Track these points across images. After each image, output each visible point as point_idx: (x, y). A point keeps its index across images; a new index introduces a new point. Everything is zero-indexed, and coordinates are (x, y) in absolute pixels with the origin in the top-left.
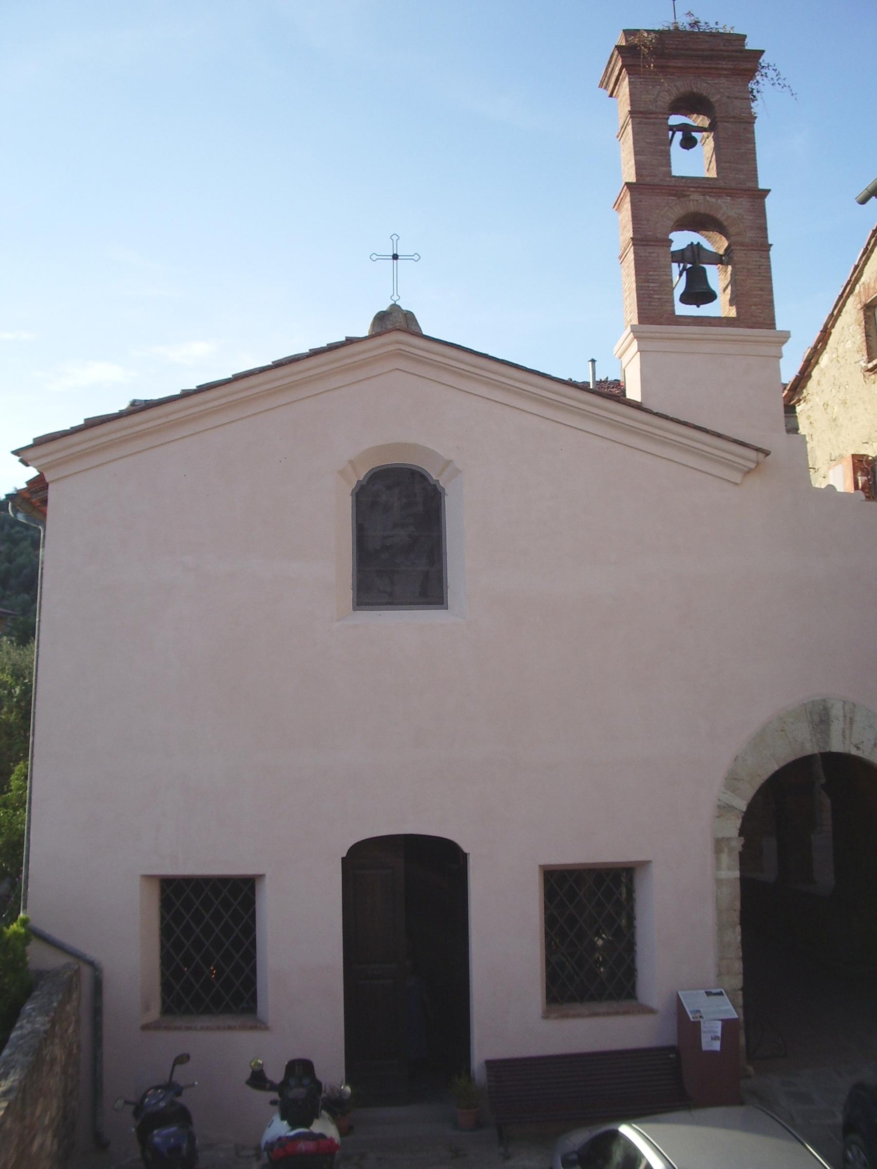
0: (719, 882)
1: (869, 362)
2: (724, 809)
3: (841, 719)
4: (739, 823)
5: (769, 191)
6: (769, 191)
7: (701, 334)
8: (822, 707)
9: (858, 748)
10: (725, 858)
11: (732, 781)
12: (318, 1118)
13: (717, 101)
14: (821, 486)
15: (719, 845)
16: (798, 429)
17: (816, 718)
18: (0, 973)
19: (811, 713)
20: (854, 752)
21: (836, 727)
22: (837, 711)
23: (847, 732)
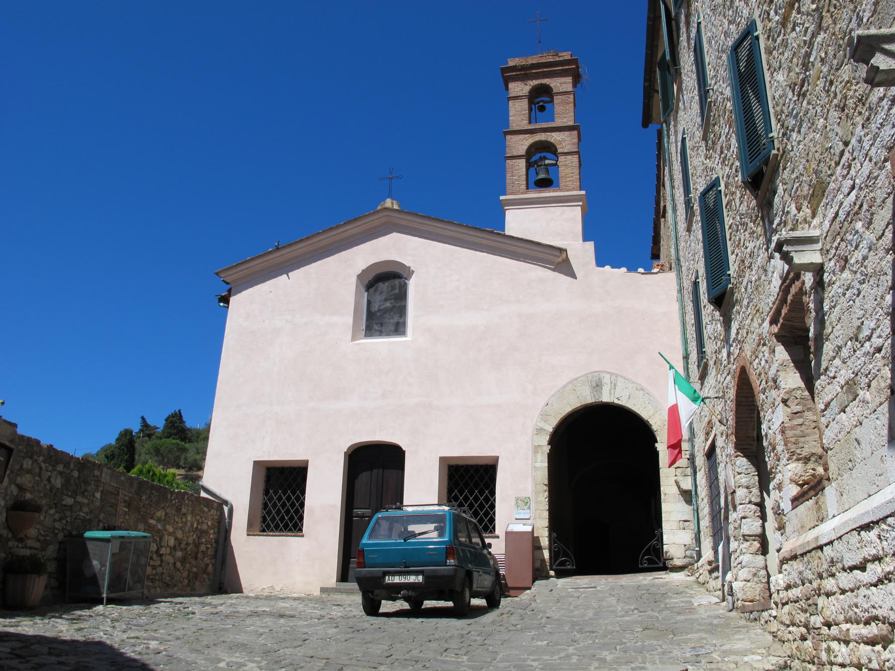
0: (535, 469)
1: (9, 441)
2: (539, 431)
3: (609, 384)
4: (548, 438)
5: (573, 275)
6: (573, 275)
7: (695, 473)
8: (597, 378)
9: (619, 399)
10: (539, 456)
11: (544, 416)
12: (651, 123)
13: (554, 86)
14: (512, 116)
15: (536, 449)
16: (878, 68)
17: (594, 385)
18: (894, 156)
19: (591, 381)
20: (616, 401)
21: (606, 389)
22: (606, 379)
23: (613, 391)
